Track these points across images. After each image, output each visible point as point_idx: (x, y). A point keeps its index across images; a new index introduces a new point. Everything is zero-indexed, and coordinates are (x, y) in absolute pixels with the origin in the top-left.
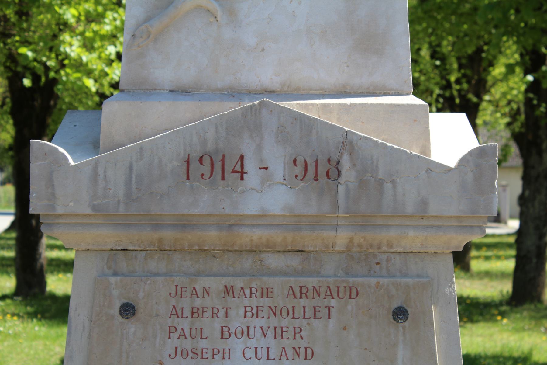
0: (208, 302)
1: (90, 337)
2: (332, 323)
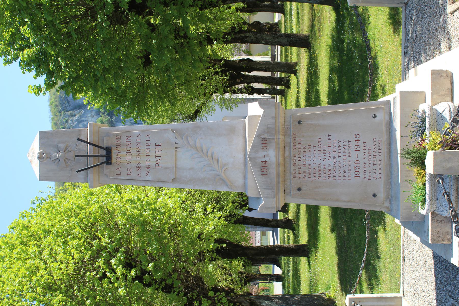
0: (297, 170)
1: (306, 199)
2: (302, 139)
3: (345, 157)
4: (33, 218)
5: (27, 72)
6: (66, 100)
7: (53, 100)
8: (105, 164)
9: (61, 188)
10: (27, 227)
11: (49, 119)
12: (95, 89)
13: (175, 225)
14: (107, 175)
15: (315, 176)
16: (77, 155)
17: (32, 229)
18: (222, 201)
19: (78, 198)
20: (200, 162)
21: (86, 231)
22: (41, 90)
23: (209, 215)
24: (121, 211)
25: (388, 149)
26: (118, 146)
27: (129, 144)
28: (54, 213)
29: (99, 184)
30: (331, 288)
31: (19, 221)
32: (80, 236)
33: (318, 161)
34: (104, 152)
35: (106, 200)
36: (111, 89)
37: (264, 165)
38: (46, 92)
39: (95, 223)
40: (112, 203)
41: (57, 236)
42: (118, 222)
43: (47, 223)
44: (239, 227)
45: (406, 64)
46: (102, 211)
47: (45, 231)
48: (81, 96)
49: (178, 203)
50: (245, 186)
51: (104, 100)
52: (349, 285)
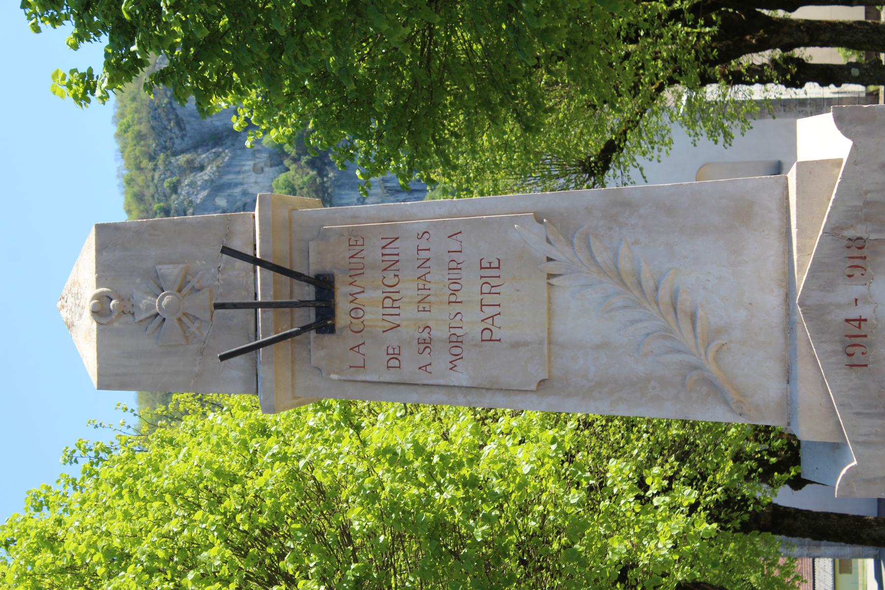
4: (72, 512)
5: (46, 27)
6: (172, 116)
7: (129, 117)
8: (313, 334)
9: (160, 409)
10: (51, 542)
11: (118, 181)
12: (271, 80)
13: (540, 537)
14: (320, 370)
16: (220, 301)
17: (69, 546)
18: (700, 455)
19: (218, 445)
20: (633, 322)
21: (245, 556)
22: (95, 85)
23: (656, 501)
24: (361, 487)
26: (356, 272)
27: (391, 265)
28: (142, 494)
29: (295, 398)
31: (25, 520)
32: (225, 571)
34: (308, 292)
35: (312, 453)
36: (323, 78)
37: (857, 332)
38: (110, 92)
39: (276, 529)
40: (328, 462)
41: (150, 571)
42: (351, 524)
43: (116, 526)
44: (758, 540)
46: (298, 488)
47: (109, 553)
48: (224, 105)
49: (551, 462)
50: (789, 404)
51: (301, 116)
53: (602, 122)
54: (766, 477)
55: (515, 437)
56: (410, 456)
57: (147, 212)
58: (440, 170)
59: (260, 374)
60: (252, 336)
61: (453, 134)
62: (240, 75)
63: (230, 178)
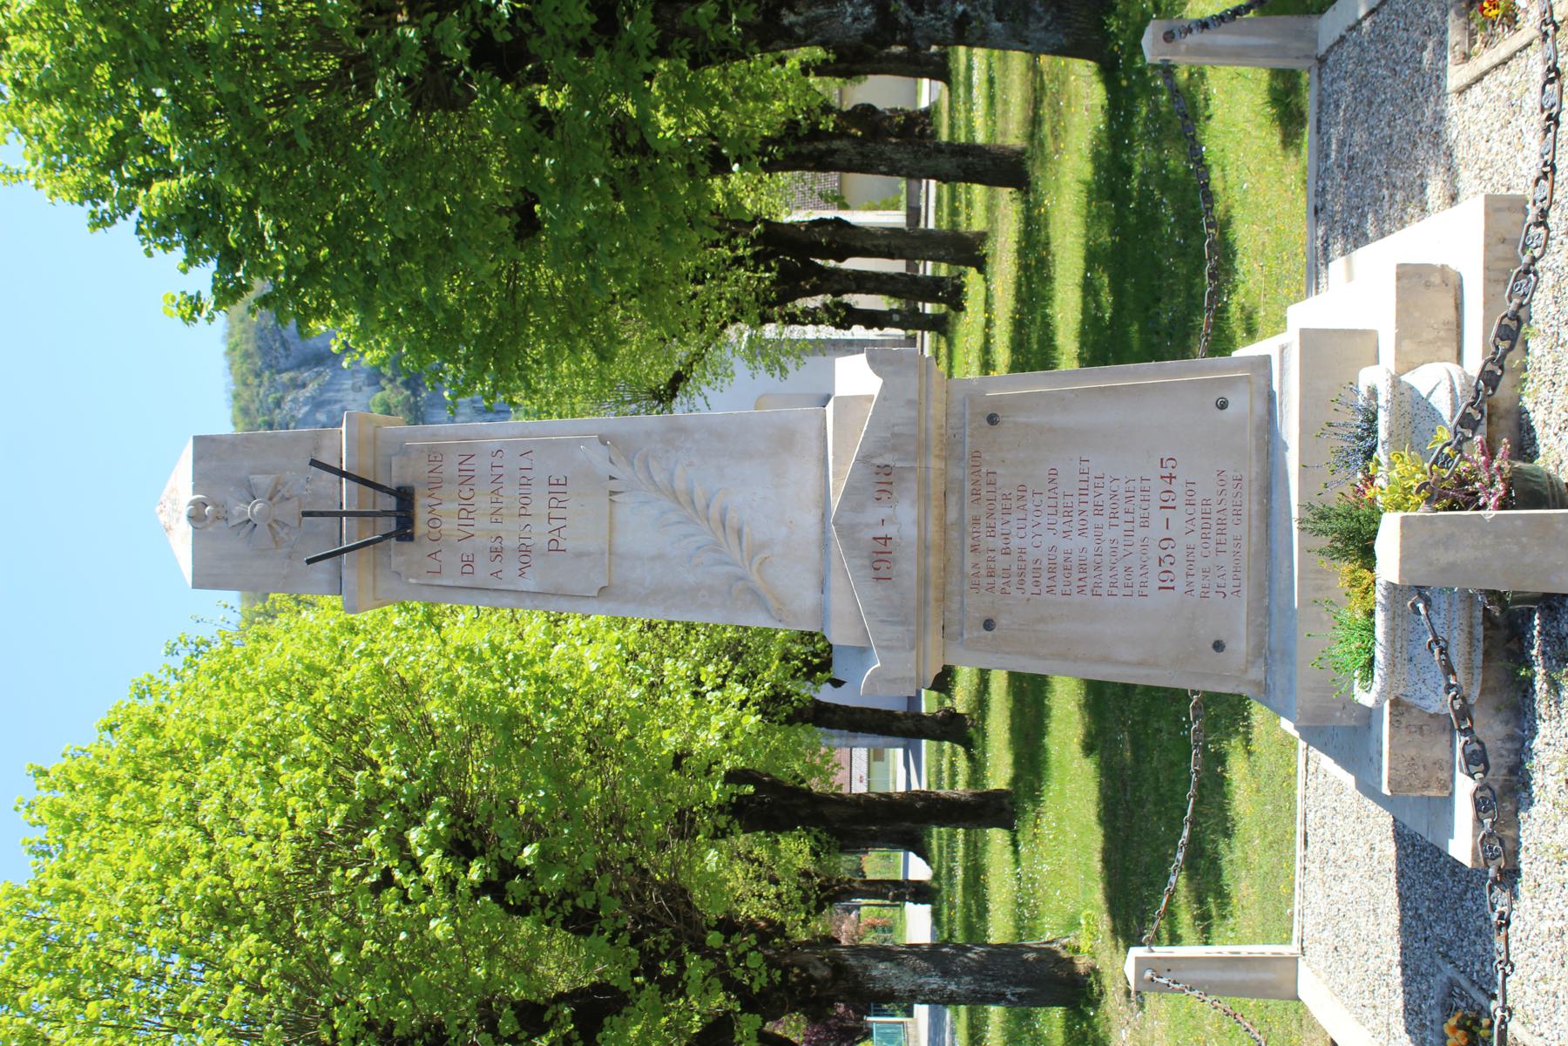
0: (983, 565)
1: (1008, 653)
3: (1129, 526)
4: (172, 701)
6: (277, 337)
7: (237, 338)
8: (393, 540)
9: (258, 607)
10: (152, 728)
12: (366, 307)
13: (606, 729)
15: (1037, 584)
16: (307, 509)
17: (170, 731)
20: (686, 537)
24: (440, 683)
25: (1260, 503)
26: (434, 485)
27: (467, 479)
28: (238, 686)
30: (1080, 924)
31: (128, 707)
32: (314, 757)
33: (1048, 539)
34: (390, 503)
35: (395, 651)
36: (415, 305)
37: (883, 549)
40: (411, 658)
41: (245, 756)
43: (213, 714)
45: (1319, 243)
46: (383, 682)
48: (323, 328)
50: (822, 611)
51: (395, 339)
52: (1138, 917)
53: (670, 355)
54: (809, 676)
55: (583, 638)
56: (487, 655)
57: (252, 426)
58: (522, 394)
59: (344, 578)
60: (337, 542)
61: (535, 361)
62: (338, 303)
63: (329, 395)
